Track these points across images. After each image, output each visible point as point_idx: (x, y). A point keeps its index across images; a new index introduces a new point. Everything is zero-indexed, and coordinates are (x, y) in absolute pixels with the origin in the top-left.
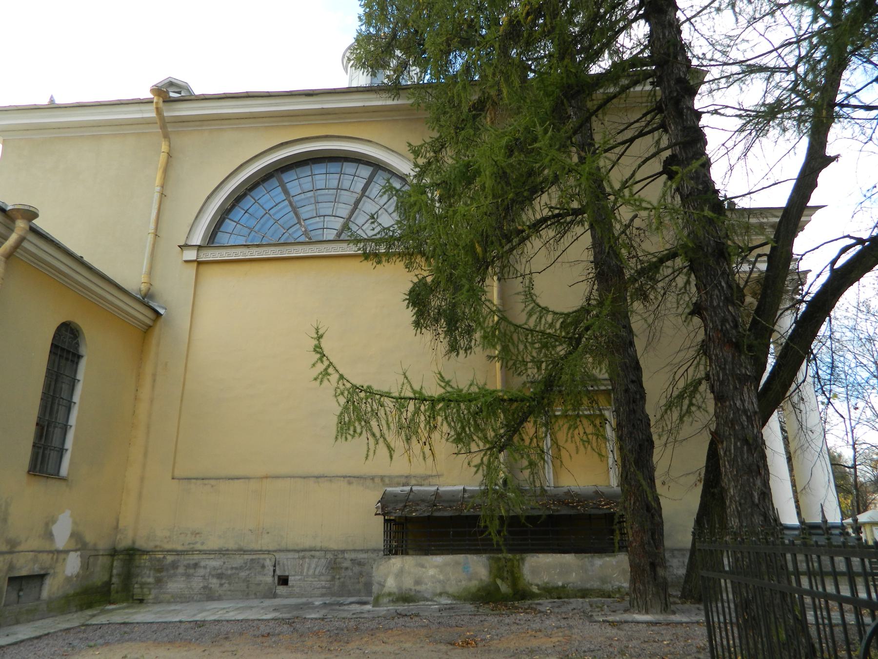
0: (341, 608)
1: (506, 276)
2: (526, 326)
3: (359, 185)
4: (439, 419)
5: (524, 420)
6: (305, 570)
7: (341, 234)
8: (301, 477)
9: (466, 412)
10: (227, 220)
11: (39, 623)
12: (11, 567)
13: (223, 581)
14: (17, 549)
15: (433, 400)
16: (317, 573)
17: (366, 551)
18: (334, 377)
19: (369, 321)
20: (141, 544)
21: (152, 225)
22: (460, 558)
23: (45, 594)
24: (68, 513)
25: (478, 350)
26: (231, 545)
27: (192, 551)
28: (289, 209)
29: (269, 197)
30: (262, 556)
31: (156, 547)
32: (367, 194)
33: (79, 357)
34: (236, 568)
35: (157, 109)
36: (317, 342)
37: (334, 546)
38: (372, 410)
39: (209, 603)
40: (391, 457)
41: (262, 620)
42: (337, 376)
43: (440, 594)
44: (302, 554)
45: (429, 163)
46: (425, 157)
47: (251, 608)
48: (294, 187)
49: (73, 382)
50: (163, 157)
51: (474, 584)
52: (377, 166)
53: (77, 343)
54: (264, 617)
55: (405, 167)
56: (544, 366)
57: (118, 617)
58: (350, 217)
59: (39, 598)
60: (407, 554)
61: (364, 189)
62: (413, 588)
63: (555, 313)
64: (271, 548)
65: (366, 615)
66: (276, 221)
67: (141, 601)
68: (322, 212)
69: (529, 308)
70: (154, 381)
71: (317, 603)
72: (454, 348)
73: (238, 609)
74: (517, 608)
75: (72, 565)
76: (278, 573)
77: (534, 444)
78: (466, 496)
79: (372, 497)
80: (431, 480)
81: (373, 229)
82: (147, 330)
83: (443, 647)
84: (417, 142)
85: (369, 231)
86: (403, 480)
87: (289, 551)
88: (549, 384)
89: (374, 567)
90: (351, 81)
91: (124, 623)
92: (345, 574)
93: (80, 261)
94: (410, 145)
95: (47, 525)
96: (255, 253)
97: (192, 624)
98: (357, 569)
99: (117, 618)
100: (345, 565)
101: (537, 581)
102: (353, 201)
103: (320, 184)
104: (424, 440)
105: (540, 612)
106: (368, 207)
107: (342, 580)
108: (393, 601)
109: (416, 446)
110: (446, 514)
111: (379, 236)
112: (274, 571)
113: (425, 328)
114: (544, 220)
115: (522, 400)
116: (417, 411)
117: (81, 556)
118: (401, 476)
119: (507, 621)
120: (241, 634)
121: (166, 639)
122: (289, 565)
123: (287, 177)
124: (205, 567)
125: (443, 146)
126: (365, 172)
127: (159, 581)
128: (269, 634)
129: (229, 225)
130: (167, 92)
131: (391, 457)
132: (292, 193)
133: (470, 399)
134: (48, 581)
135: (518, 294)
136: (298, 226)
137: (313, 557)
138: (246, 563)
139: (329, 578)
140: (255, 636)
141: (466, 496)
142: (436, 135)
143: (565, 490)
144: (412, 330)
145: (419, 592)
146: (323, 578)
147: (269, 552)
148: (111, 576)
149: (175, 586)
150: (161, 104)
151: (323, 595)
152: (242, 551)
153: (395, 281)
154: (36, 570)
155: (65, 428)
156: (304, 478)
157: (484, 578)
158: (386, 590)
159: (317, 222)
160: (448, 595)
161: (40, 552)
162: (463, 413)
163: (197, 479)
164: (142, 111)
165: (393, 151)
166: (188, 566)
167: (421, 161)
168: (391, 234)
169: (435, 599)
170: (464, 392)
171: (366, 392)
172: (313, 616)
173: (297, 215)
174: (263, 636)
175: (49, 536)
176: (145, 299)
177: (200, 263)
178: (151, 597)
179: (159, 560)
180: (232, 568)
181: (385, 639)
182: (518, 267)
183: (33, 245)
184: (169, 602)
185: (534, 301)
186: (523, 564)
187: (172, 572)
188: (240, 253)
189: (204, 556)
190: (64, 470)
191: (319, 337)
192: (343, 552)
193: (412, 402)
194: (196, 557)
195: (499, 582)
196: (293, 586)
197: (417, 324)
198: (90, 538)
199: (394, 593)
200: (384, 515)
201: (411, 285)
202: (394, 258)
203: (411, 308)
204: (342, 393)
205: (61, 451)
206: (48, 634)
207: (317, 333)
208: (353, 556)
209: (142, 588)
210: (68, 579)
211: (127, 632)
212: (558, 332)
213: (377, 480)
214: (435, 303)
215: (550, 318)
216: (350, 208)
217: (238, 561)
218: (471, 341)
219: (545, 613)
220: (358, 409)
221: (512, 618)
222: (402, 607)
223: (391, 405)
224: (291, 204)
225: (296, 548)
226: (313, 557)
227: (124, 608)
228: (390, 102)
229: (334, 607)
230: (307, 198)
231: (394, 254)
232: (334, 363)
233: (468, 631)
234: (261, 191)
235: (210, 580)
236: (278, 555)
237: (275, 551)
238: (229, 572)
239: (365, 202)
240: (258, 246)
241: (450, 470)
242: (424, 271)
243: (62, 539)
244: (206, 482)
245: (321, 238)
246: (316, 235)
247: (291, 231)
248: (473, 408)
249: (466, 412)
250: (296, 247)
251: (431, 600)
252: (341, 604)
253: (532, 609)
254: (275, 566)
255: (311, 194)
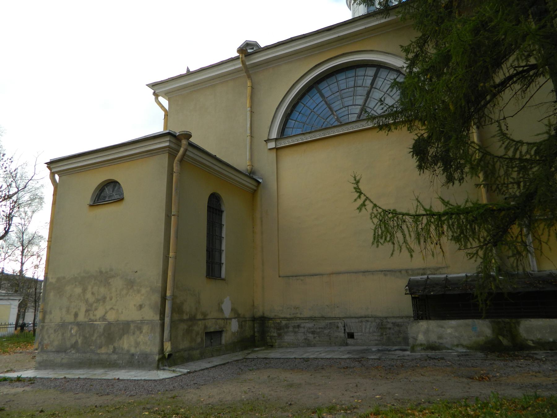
0: (390, 353)
1: (483, 124)
2: (506, 156)
3: (369, 81)
4: (445, 227)
5: (512, 222)
6: (364, 329)
7: (360, 116)
8: (353, 273)
9: (464, 221)
10: (290, 120)
11: (223, 357)
12: (206, 327)
13: (315, 336)
14: (208, 317)
15: (440, 215)
16: (371, 331)
17: (402, 317)
18: (369, 206)
19: (389, 168)
20: (267, 314)
21: (249, 131)
22: (469, 321)
23: (223, 342)
24: (228, 297)
25: (467, 178)
26: (317, 314)
27: (295, 318)
28: (325, 106)
29: (313, 101)
30: (336, 321)
31: (275, 316)
32: (374, 86)
33: (222, 212)
34: (322, 328)
35: (242, 61)
36: (355, 186)
37: (379, 314)
38: (398, 225)
39: (309, 348)
40: (412, 256)
41: (342, 359)
42: (371, 205)
43: (457, 346)
44: (360, 319)
45: (417, 56)
46: (413, 52)
47: (334, 351)
48: (326, 92)
49: (221, 226)
50: (249, 90)
51: (482, 339)
52: (379, 66)
53: (220, 205)
54: (343, 357)
55: (399, 63)
56: (522, 184)
57: (261, 355)
58: (365, 103)
59: (221, 344)
60: (430, 319)
61: (372, 84)
62: (437, 341)
63: (528, 144)
64: (341, 316)
65: (407, 358)
66: (319, 115)
67: (272, 346)
68: (346, 104)
69: (506, 144)
70: (262, 221)
71: (374, 350)
72: (450, 179)
73: (326, 352)
74: (517, 356)
75: (234, 326)
76: (347, 331)
77: (519, 240)
78: (469, 280)
79: (402, 283)
80: (441, 270)
81: (383, 109)
82: (254, 192)
83: (464, 380)
84: (406, 44)
85: (379, 111)
86: (421, 272)
87: (352, 318)
88: (529, 197)
89: (409, 327)
90: (354, 14)
91: (265, 358)
92: (390, 332)
93: (214, 158)
94: (402, 46)
95: (219, 304)
96: (309, 138)
97: (302, 360)
98: (397, 328)
99: (261, 355)
100: (389, 326)
101: (532, 338)
102: (365, 93)
103: (343, 86)
104: (435, 242)
105: (537, 359)
106: (376, 95)
107: (388, 335)
108: (424, 349)
109: (430, 247)
110: (455, 292)
111: (386, 113)
112: (345, 330)
113: (426, 169)
114: (510, 78)
115: (509, 209)
116: (428, 224)
117: (238, 321)
118: (420, 269)
119: (511, 364)
120: (331, 366)
121: (289, 368)
122: (353, 326)
123: (322, 86)
124: (304, 327)
125: (425, 42)
126: (371, 72)
127: (280, 335)
128: (347, 367)
129: (291, 123)
130: (246, 50)
131: (412, 256)
132: (326, 96)
133: (466, 211)
134: (224, 335)
135: (494, 136)
136: (332, 116)
137: (368, 321)
138: (327, 325)
139: (379, 334)
140: (339, 368)
141: (469, 280)
142: (420, 34)
143: (548, 273)
144: (417, 172)
145: (442, 343)
146: (375, 334)
147: (340, 318)
148: (254, 332)
149: (289, 338)
150: (244, 58)
151: (377, 345)
152: (324, 318)
153: (402, 140)
154: (217, 328)
155: (220, 252)
156: (356, 273)
157: (489, 335)
158: (418, 342)
159: (344, 111)
160: (463, 346)
161: (218, 319)
162: (460, 222)
163: (293, 276)
164: (234, 65)
165: (389, 53)
166: (294, 327)
167: (411, 56)
168: (395, 109)
169: (454, 348)
170: (462, 207)
171: (392, 213)
172: (373, 357)
173: (331, 109)
174: (344, 368)
175: (221, 310)
176: (251, 175)
177: (277, 149)
178: (276, 344)
179: (278, 323)
180: (319, 328)
181: (423, 373)
182: (492, 116)
183: (192, 153)
184: (287, 347)
185: (509, 138)
186: (519, 326)
187: (286, 330)
188: (300, 140)
189: (303, 321)
190: (223, 275)
191: (357, 182)
192: (386, 318)
193: (425, 218)
194: (298, 321)
195: (501, 338)
196: (357, 339)
197: (420, 167)
198: (241, 311)
199: (424, 344)
200: (411, 294)
201: (414, 142)
202: (400, 126)
203: (415, 157)
204: (376, 216)
205: (220, 264)
206: (228, 363)
207: (355, 180)
208: (394, 320)
209: (271, 339)
210: (233, 333)
211: (267, 363)
212: (533, 157)
213: (403, 272)
214: (432, 151)
215: (524, 149)
216: (364, 98)
217: (323, 324)
218: (463, 174)
219: (541, 360)
220: (387, 224)
221: (515, 363)
222: (431, 353)
223: (411, 220)
224: (326, 103)
225: (356, 316)
226: (368, 321)
227: (264, 350)
228: (383, 21)
229: (385, 352)
230: (336, 97)
231: (400, 122)
232: (369, 197)
233: (482, 370)
234: (307, 97)
235: (308, 335)
236: (345, 320)
237: (344, 318)
238: (318, 330)
239: (373, 92)
240: (310, 133)
241: (455, 262)
242: (422, 131)
243: (227, 313)
244: (298, 278)
245: (347, 121)
246: (344, 120)
247: (328, 120)
248: (470, 218)
249: (464, 221)
250: (333, 130)
251: (451, 349)
252: (389, 351)
253: (530, 357)
254: (344, 327)
255: (338, 94)
